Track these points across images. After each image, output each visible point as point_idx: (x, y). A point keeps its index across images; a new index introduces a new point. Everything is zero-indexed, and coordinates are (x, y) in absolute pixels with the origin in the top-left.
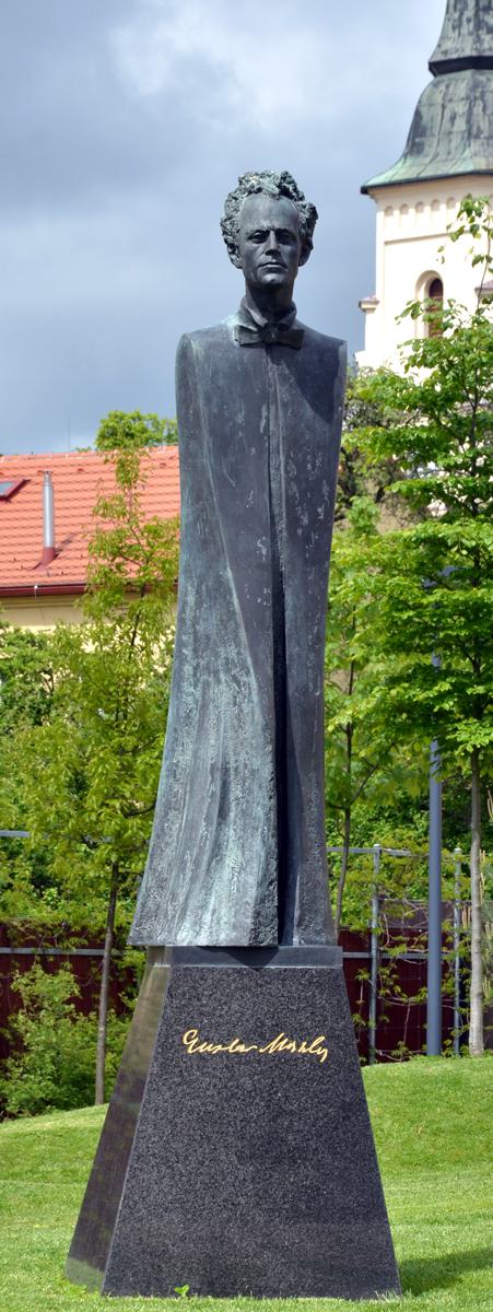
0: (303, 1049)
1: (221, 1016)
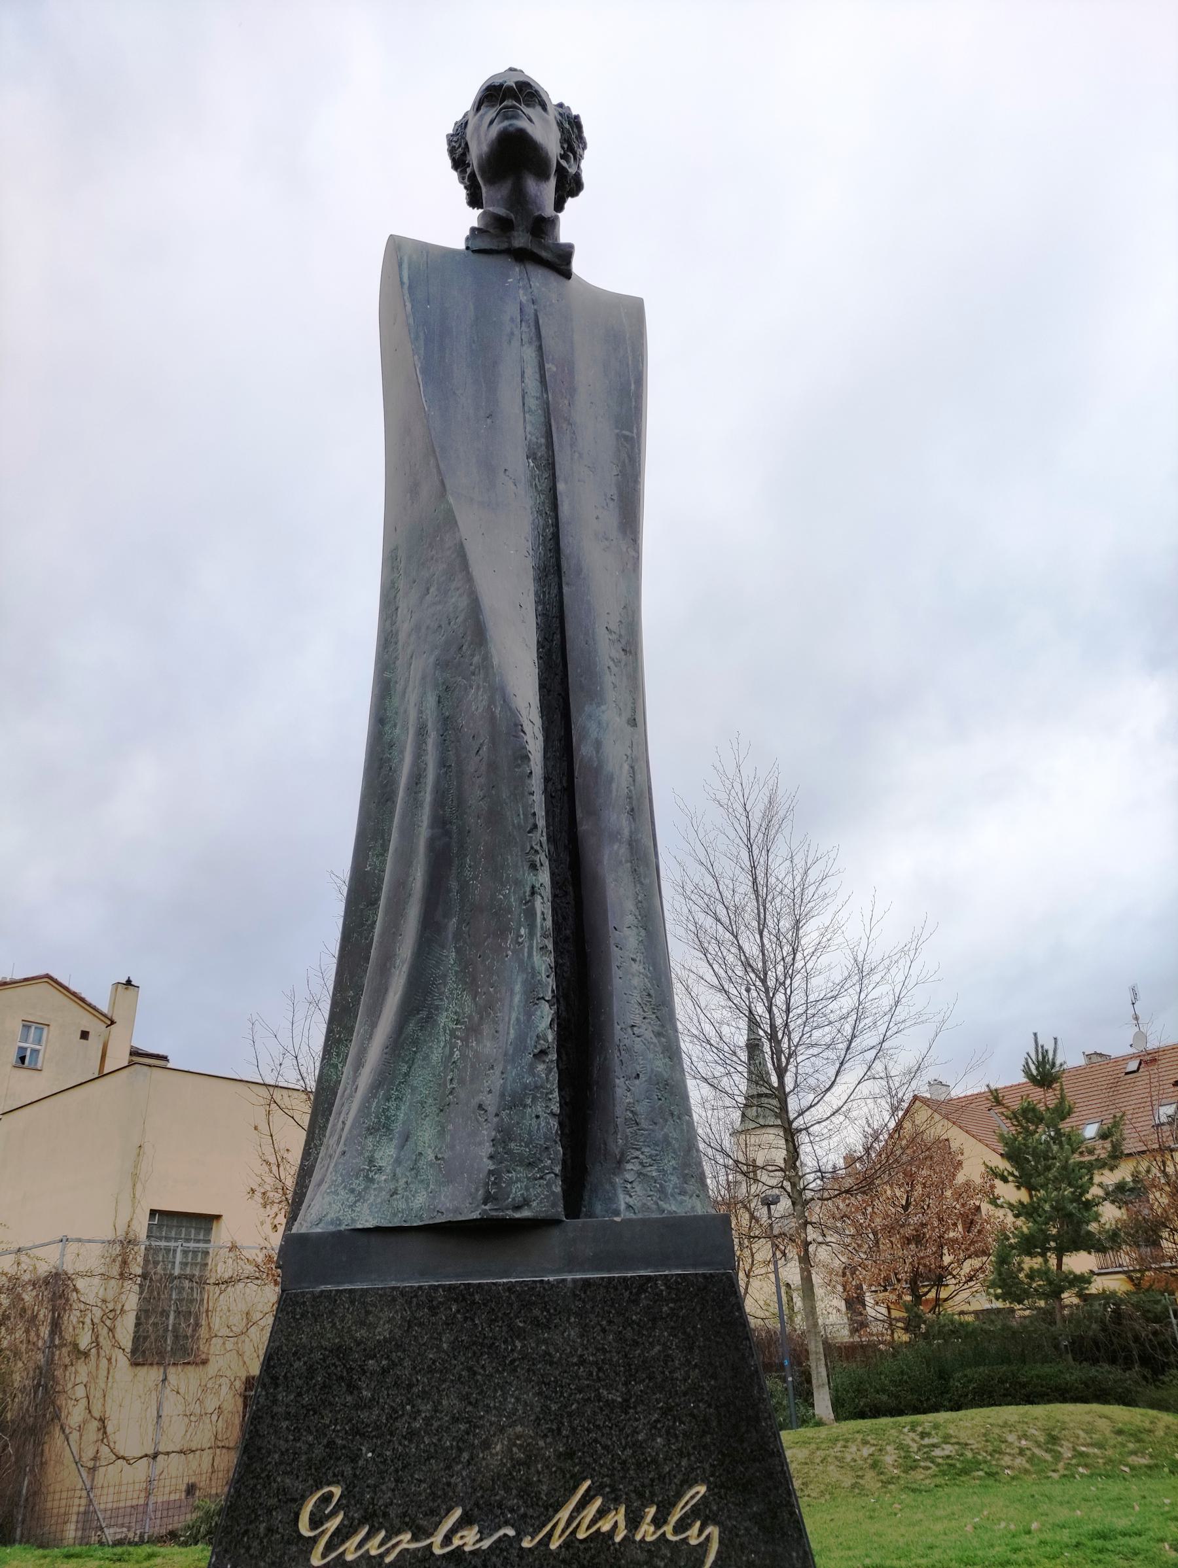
0: (647, 1532)
1: (412, 1434)
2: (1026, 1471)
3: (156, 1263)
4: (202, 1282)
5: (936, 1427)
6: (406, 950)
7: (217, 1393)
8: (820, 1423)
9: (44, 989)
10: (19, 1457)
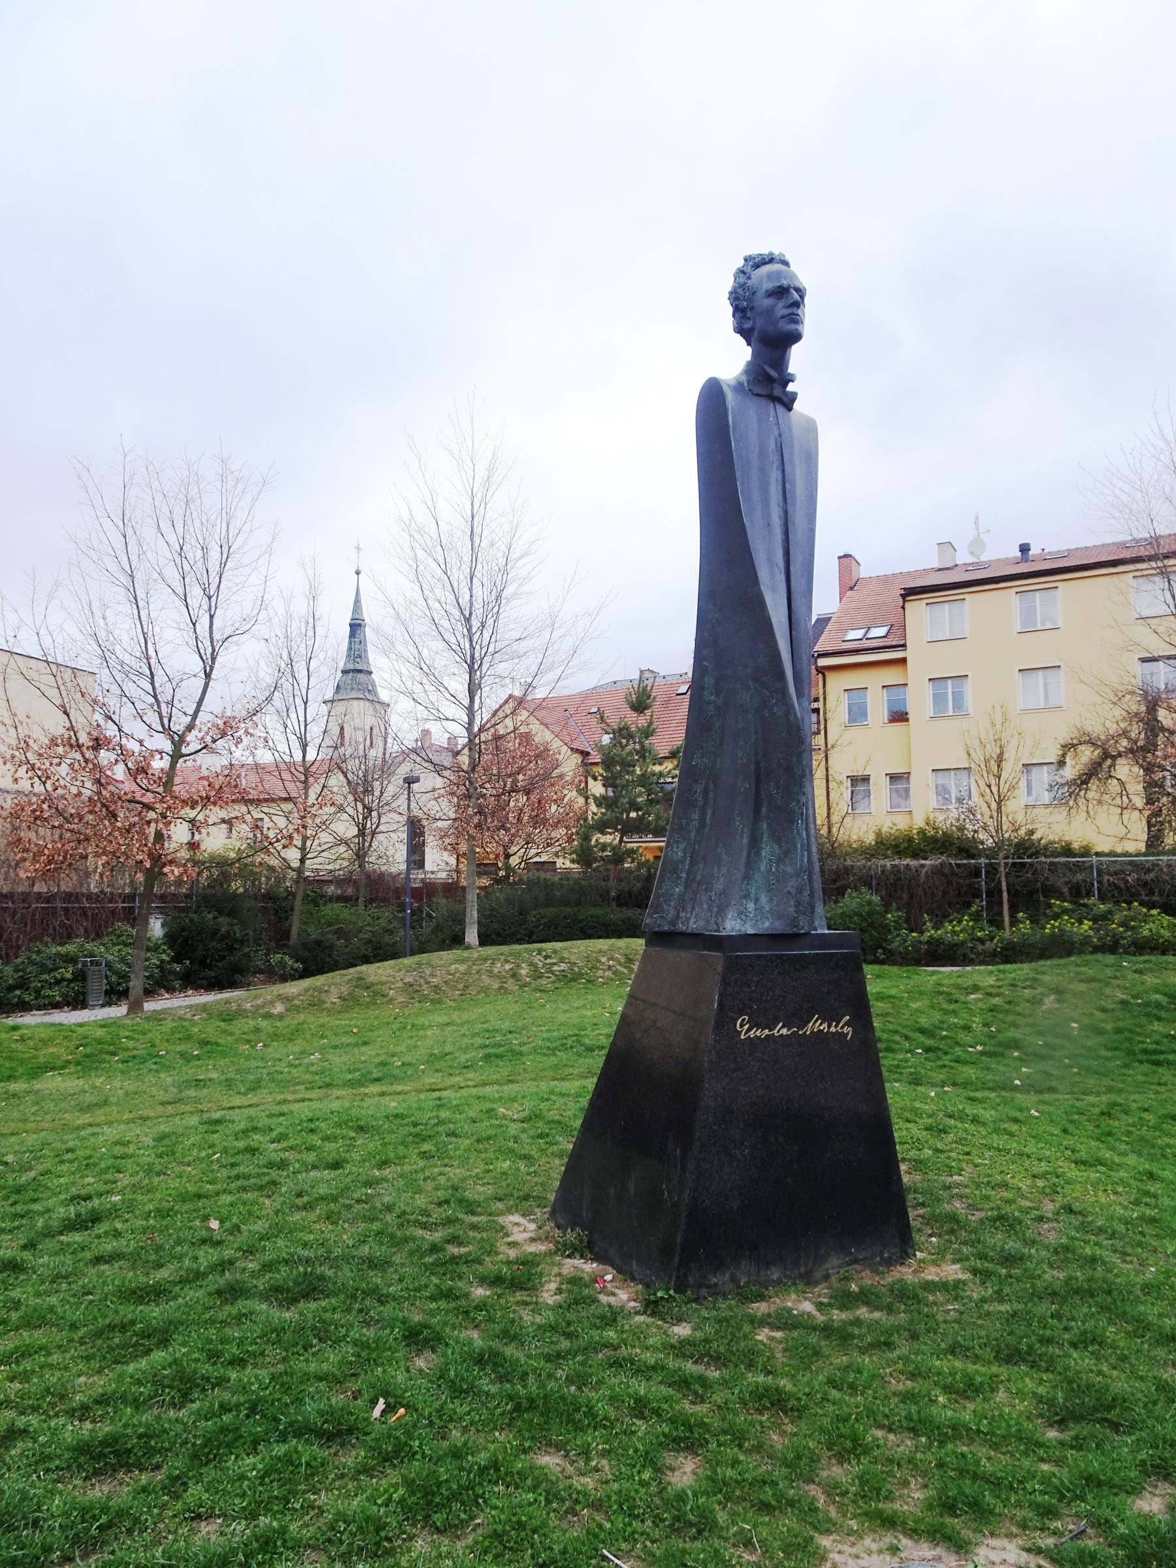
0: (833, 1029)
1: (767, 1001)
5: (555, 952)
8: (469, 948)
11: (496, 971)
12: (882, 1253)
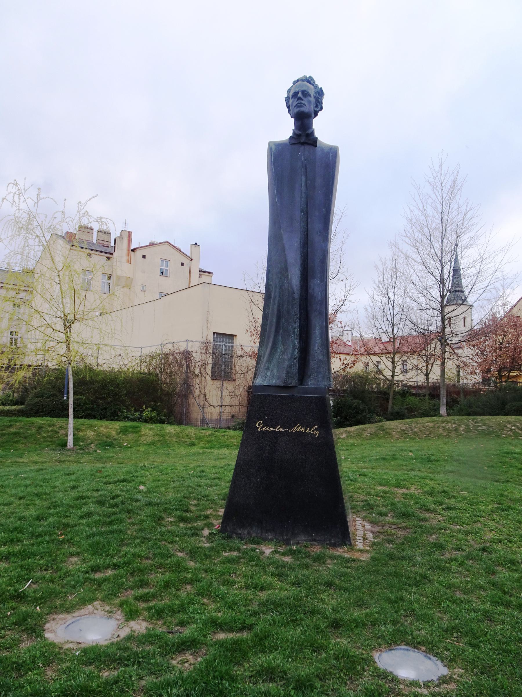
0: (308, 431)
1: (273, 415)
2: (511, 436)
3: (217, 349)
4: (232, 356)
6: (271, 339)
7: (239, 390)
8: (441, 416)
9: (166, 246)
10: (182, 402)
11: (447, 427)
12: (330, 540)
